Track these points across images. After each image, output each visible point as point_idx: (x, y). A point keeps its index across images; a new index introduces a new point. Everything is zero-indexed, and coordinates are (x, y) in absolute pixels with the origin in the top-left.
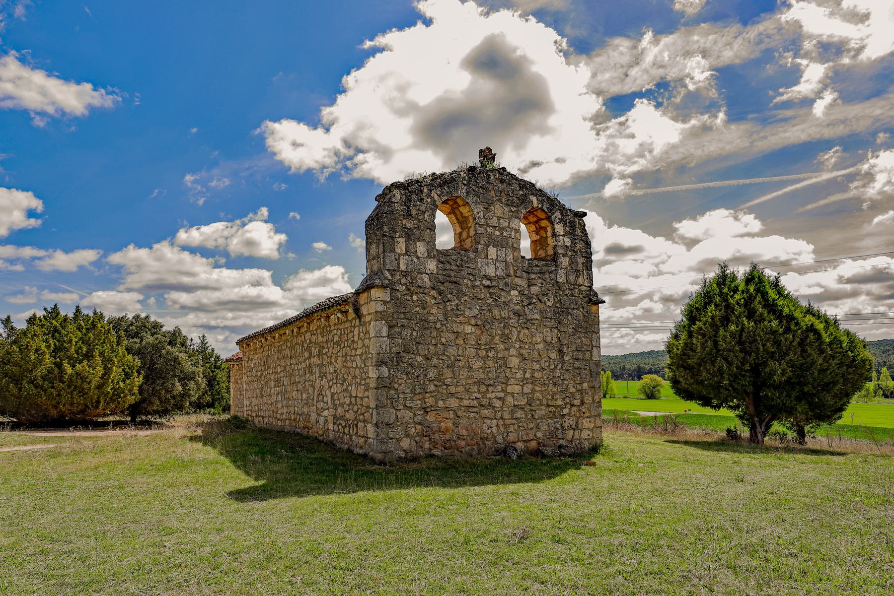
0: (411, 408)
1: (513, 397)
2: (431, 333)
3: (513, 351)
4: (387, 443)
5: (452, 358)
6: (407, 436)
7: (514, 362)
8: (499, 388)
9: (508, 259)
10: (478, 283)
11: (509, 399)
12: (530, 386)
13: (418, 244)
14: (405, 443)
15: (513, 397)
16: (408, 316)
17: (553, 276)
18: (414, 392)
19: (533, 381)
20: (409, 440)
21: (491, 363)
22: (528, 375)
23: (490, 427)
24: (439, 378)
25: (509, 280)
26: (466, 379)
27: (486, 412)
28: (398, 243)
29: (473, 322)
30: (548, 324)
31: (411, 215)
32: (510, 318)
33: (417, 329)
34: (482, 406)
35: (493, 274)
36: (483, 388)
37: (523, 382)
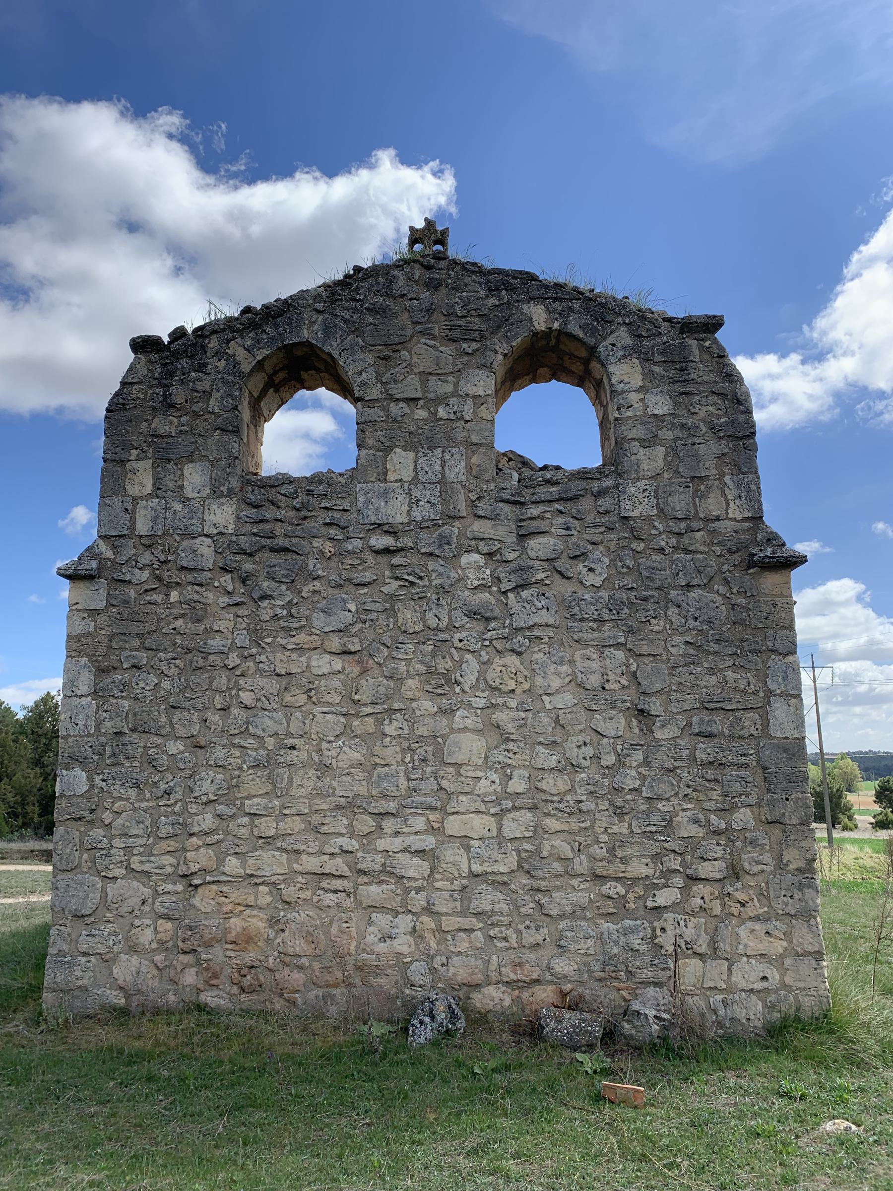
0: (147, 874)
1: (468, 848)
2: (211, 679)
3: (462, 718)
4: (71, 965)
5: (270, 742)
6: (134, 949)
7: (469, 747)
8: (419, 823)
9: (451, 475)
10: (355, 544)
11: (453, 855)
12: (527, 817)
13: (188, 469)
14: (126, 969)
15: (468, 848)
16: (150, 642)
17: (605, 503)
18: (153, 832)
19: (537, 802)
20: (135, 960)
21: (391, 753)
22: (517, 785)
23: (388, 940)
24: (229, 793)
25: (454, 529)
26: (311, 797)
27: (373, 892)
28: (134, 472)
29: (335, 643)
30: (587, 636)
31: (172, 406)
32: (453, 627)
33: (173, 671)
34: (362, 872)
35: (401, 518)
36: (366, 823)
37: (502, 806)
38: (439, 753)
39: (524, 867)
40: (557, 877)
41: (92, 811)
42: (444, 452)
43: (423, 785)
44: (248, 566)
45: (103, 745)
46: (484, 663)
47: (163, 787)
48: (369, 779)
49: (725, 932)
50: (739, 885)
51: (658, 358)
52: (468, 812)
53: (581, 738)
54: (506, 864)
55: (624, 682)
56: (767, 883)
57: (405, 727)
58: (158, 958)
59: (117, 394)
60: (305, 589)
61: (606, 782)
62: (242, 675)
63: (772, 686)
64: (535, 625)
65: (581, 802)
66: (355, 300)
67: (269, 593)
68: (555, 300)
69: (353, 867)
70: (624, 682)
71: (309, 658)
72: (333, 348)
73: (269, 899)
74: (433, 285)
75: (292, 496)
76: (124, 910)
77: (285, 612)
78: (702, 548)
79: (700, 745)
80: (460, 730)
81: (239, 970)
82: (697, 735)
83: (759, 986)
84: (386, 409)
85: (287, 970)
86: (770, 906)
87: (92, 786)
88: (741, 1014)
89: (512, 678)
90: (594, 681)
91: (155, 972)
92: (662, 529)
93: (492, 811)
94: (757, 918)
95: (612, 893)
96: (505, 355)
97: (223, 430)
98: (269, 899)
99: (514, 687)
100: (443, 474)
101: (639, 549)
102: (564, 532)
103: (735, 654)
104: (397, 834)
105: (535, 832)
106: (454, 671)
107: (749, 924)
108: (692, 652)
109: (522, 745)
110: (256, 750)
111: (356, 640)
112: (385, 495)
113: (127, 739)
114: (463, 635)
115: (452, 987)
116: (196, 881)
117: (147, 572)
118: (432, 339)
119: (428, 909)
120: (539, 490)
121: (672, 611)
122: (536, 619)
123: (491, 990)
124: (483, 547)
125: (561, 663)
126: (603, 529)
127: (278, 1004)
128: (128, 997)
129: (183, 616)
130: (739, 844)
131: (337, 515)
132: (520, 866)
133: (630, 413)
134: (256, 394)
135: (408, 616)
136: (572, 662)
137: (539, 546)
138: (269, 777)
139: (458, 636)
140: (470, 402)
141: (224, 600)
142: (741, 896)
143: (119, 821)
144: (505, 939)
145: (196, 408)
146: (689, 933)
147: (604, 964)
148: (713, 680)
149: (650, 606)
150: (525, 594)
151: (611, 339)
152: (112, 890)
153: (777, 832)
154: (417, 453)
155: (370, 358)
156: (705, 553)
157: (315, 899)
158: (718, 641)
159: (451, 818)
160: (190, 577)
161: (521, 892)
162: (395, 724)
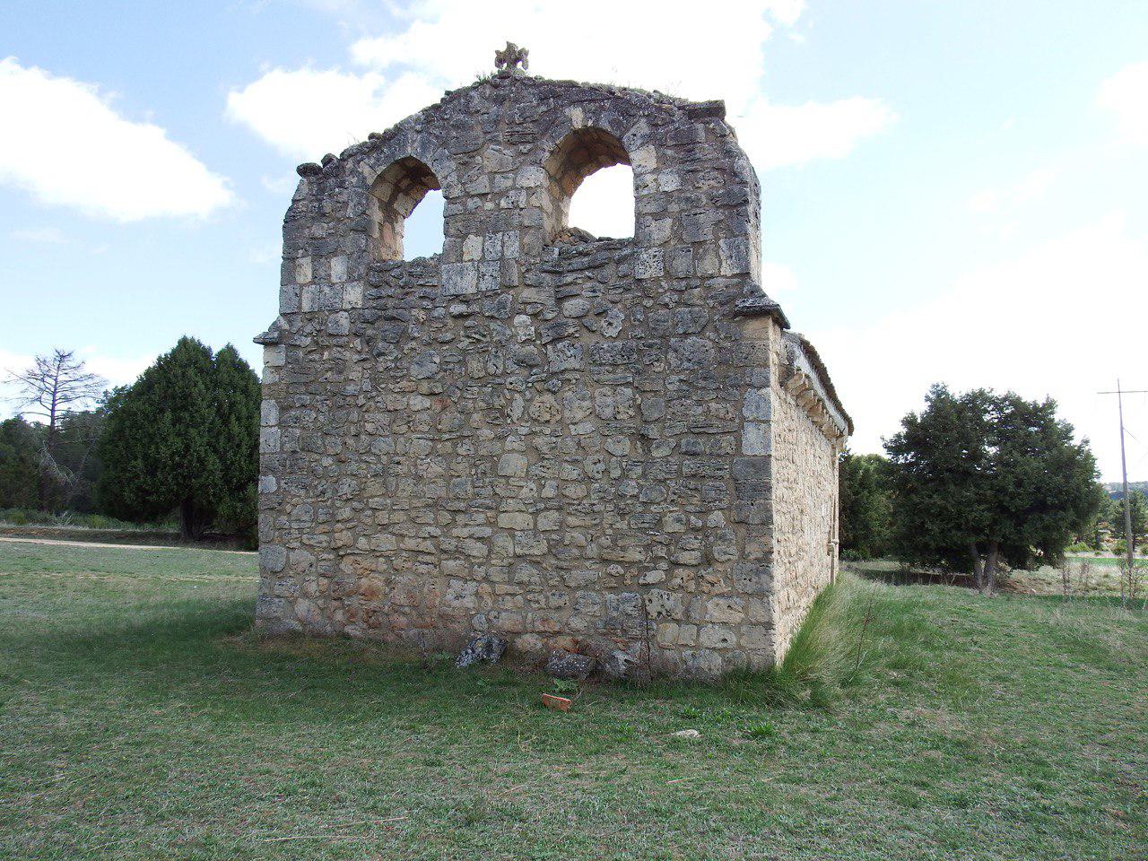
0: (311, 546)
1: (513, 537)
3: (511, 443)
5: (384, 458)
6: (306, 595)
7: (515, 463)
8: (480, 518)
9: (508, 253)
10: (441, 311)
11: (504, 543)
12: (554, 515)
14: (302, 607)
15: (513, 537)
16: (312, 388)
17: (623, 268)
21: (461, 467)
23: (459, 598)
24: (359, 495)
25: (508, 297)
26: (410, 497)
27: (451, 565)
28: (300, 266)
31: (324, 215)
32: (505, 374)
33: (325, 409)
35: (472, 290)
36: (445, 517)
37: (537, 507)
38: (494, 467)
39: (552, 551)
40: (575, 559)
41: (280, 504)
42: (503, 235)
43: (483, 491)
44: (370, 332)
45: (285, 460)
46: (528, 401)
47: (320, 488)
48: (447, 486)
49: (697, 605)
50: (710, 570)
51: (670, 143)
52: (513, 511)
53: (596, 457)
54: (539, 549)
55: (631, 412)
56: (732, 569)
57: (472, 449)
58: (320, 602)
59: (290, 209)
60: (406, 347)
61: (613, 490)
62: (366, 411)
63: (746, 413)
64: (566, 370)
65: (594, 505)
66: (443, 119)
67: (382, 351)
68: (591, 101)
69: (437, 547)
70: (631, 412)
71: (409, 399)
72: (427, 160)
73: (385, 567)
74: (500, 101)
75: (398, 278)
76: (299, 570)
77: (393, 365)
78: (698, 302)
79: (687, 462)
80: (509, 452)
81: (367, 613)
82: (686, 453)
83: (720, 645)
84: (464, 204)
85: (396, 615)
86: (733, 587)
87: (279, 488)
88: (704, 664)
89: (547, 412)
90: (608, 412)
91: (319, 611)
92: (666, 288)
93: (530, 510)
94: (722, 595)
95: (613, 572)
96: (552, 153)
97: (357, 231)
98: (385, 567)
99: (548, 418)
100: (502, 252)
101: (648, 305)
102: (591, 294)
103: (718, 388)
104: (466, 525)
105: (561, 527)
106: (507, 407)
107: (715, 599)
108: (685, 387)
109: (553, 462)
110: (376, 464)
111: (438, 384)
112: (461, 273)
113: (298, 456)
114: (512, 379)
115: (502, 633)
116: (341, 553)
117: (309, 338)
118: (498, 145)
119: (486, 579)
120: (573, 261)
121: (671, 355)
122: (567, 365)
123: (527, 637)
124: (529, 310)
125: (583, 399)
126: (621, 290)
127: (391, 638)
128: (304, 625)
129: (331, 369)
130: (711, 538)
131: (428, 290)
132: (550, 551)
133: (645, 192)
134: (386, 200)
135: (475, 365)
136: (592, 398)
137: (572, 307)
138: (384, 483)
139: (509, 380)
140: (524, 193)
141: (356, 357)
142: (710, 578)
143: (295, 511)
144: (538, 602)
145: (338, 215)
146: (669, 604)
147: (606, 623)
148: (700, 410)
149: (654, 352)
150: (560, 346)
151: (633, 130)
152: (292, 556)
153: (742, 531)
154: (484, 237)
155: (453, 165)
156: (701, 306)
157: (414, 568)
158: (705, 379)
159: (502, 515)
160: (335, 342)
161: (550, 569)
162: (465, 446)
